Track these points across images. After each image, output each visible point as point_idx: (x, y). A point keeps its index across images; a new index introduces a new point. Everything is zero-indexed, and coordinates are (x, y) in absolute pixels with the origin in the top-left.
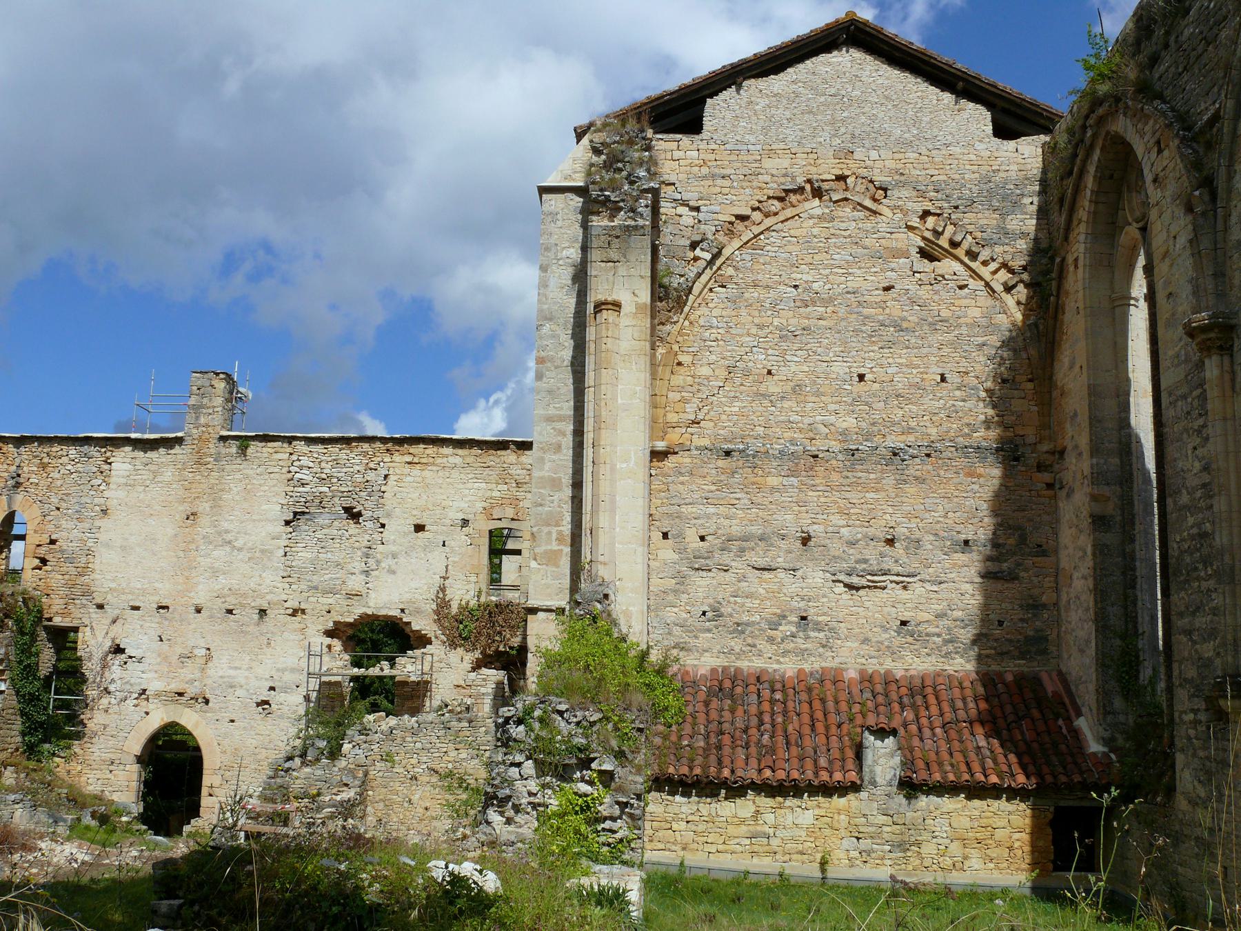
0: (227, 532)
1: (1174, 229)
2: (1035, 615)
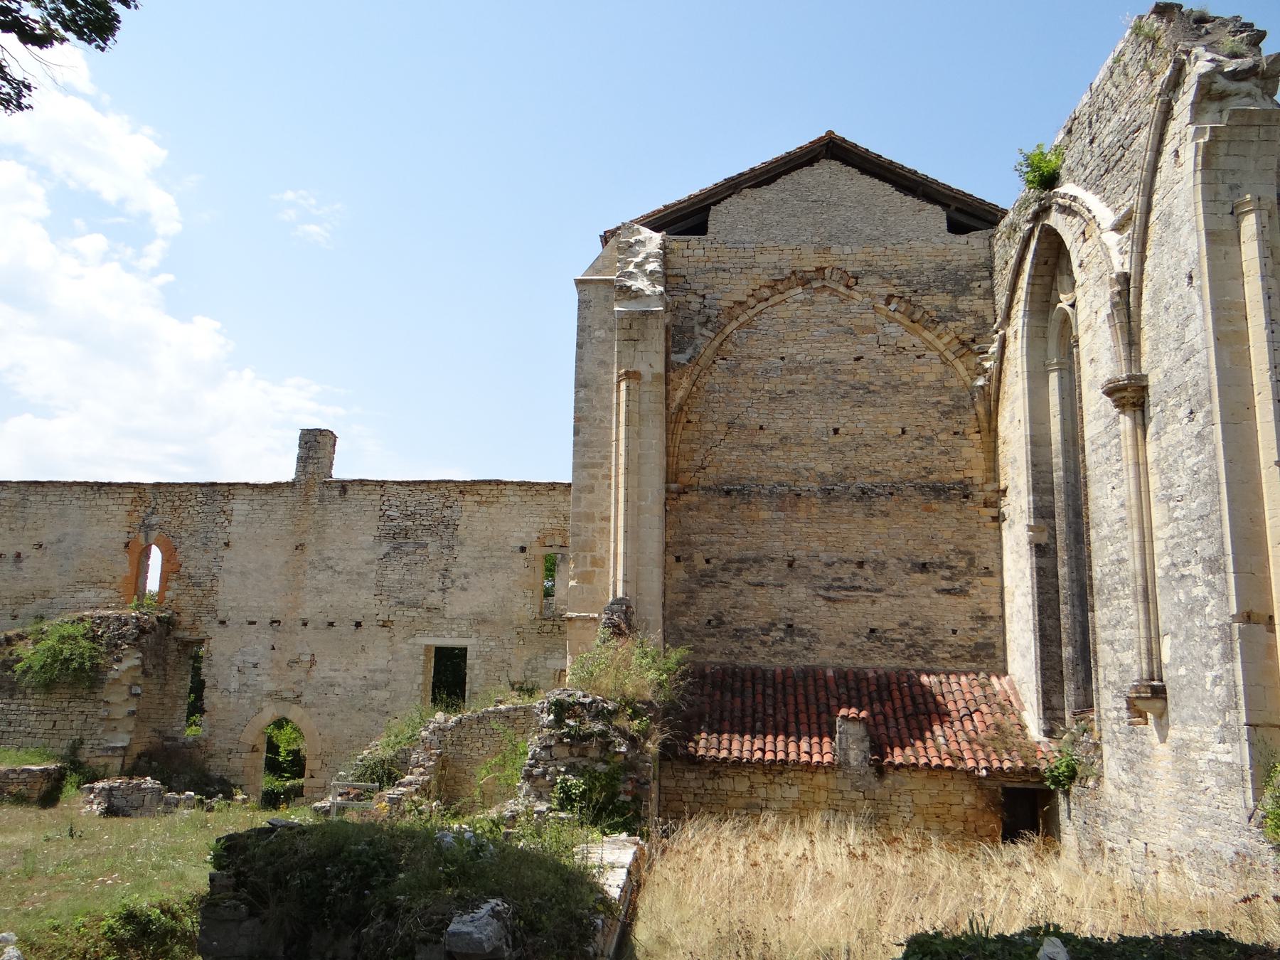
0: (329, 558)
1: (1096, 305)
2: (983, 626)
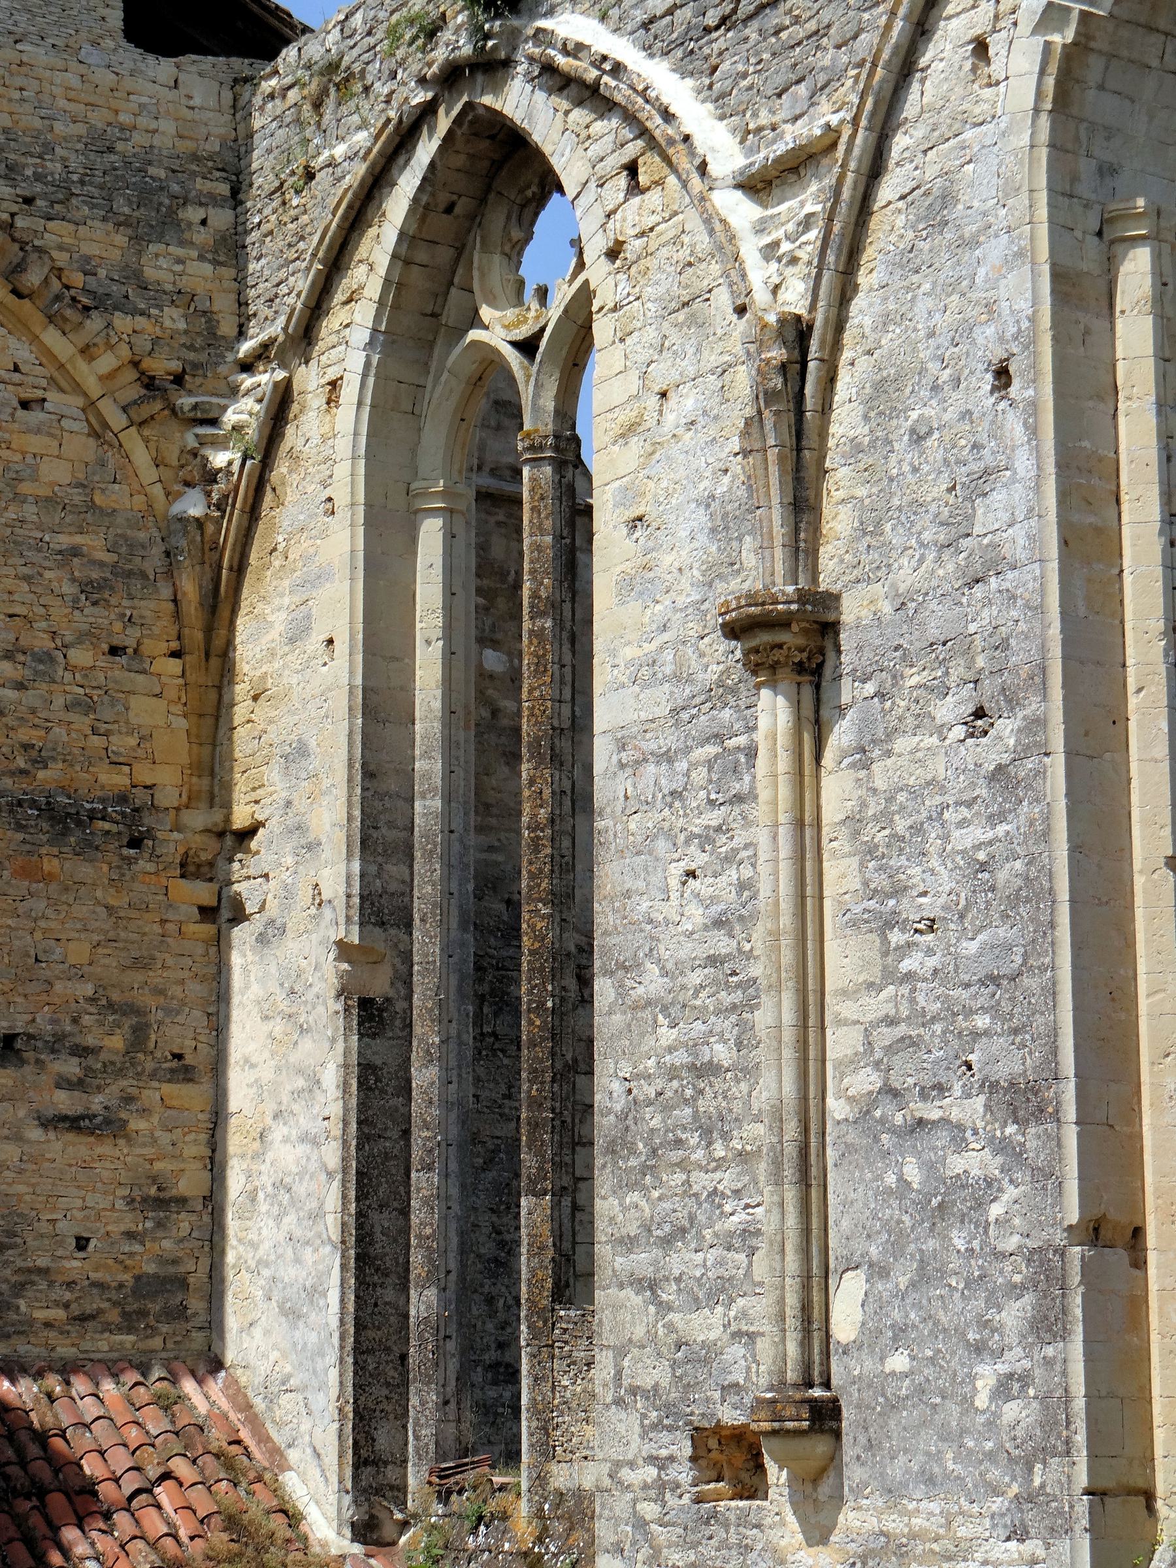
2: (160, 1224)
